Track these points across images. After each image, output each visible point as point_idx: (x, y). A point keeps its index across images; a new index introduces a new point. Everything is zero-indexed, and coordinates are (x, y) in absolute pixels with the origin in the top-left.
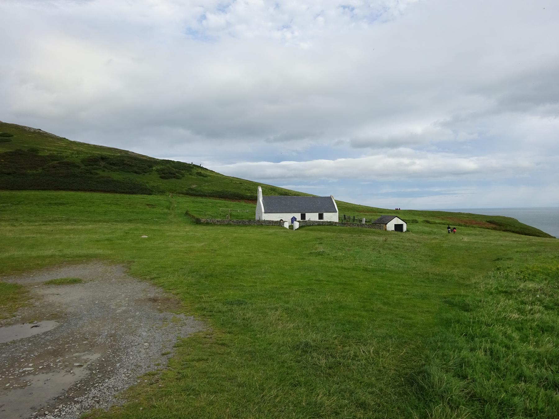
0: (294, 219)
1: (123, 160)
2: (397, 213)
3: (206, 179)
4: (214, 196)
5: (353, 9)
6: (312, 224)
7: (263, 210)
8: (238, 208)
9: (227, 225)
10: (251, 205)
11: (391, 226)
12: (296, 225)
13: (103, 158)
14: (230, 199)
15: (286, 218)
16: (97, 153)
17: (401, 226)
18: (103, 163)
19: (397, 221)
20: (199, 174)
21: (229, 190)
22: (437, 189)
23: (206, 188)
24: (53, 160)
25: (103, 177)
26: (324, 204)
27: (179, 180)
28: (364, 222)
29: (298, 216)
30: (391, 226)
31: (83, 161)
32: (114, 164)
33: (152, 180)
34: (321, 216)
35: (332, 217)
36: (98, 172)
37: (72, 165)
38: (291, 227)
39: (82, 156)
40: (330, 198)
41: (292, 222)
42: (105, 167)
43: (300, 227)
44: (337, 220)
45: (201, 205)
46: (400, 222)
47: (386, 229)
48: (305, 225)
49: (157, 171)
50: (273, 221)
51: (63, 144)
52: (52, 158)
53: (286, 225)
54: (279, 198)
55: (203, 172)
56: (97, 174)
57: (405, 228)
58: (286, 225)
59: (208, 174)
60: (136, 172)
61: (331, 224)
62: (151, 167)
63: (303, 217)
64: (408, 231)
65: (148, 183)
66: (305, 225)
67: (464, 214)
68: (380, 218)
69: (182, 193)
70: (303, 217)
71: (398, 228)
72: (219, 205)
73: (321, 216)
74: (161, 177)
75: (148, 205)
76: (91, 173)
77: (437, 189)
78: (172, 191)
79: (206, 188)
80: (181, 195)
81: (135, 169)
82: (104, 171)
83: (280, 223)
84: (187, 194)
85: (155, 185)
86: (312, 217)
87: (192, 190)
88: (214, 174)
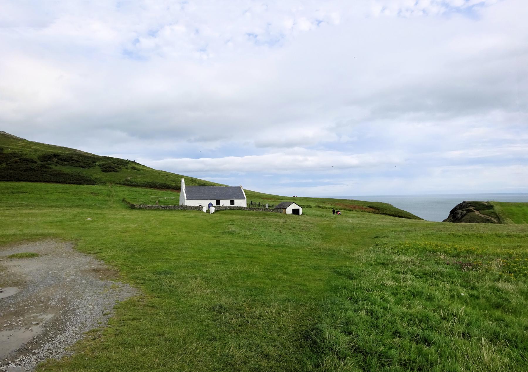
0: (210, 205)
1: (72, 157)
2: (294, 199)
3: (139, 172)
4: (145, 186)
5: (256, 36)
6: (225, 209)
7: (186, 198)
8: (165, 196)
9: (156, 210)
10: (175, 193)
11: (289, 210)
12: (213, 210)
13: (56, 156)
14: (158, 188)
15: (204, 203)
16: (51, 151)
17: (298, 209)
18: (55, 160)
19: (294, 206)
20: (134, 168)
21: (158, 181)
22: (327, 180)
23: (139, 179)
24: (15, 157)
25: (55, 171)
26: (234, 193)
27: (117, 173)
28: (267, 207)
29: (214, 202)
30: (289, 210)
31: (39, 158)
32: (65, 160)
33: (95, 173)
34: (232, 203)
36: (51, 166)
37: (27, 161)
38: (208, 211)
39: (38, 154)
40: (239, 188)
41: (209, 207)
42: (57, 162)
43: (216, 211)
45: (135, 193)
46: (296, 207)
47: (285, 213)
48: (220, 210)
49: (100, 165)
50: (193, 207)
51: (23, 144)
52: (14, 155)
53: (205, 210)
54: (199, 187)
55: (136, 166)
56: (50, 168)
57: (301, 212)
58: (205, 210)
59: (141, 168)
60: (82, 167)
61: (240, 208)
62: (94, 162)
63: (218, 203)
64: (303, 214)
65: (92, 175)
66: (220, 210)
67: (349, 200)
68: (279, 204)
69: (120, 184)
70: (218, 203)
71: (296, 212)
72: (149, 193)
73: (232, 203)
74: (103, 171)
75: (92, 193)
76: (46, 168)
77: (327, 180)
78: (112, 182)
79: (139, 179)
80: (119, 185)
81: (82, 164)
82: (56, 166)
83: (199, 208)
84: (124, 184)
85: (98, 177)
86: (225, 203)
87: (128, 181)
88: (146, 168)
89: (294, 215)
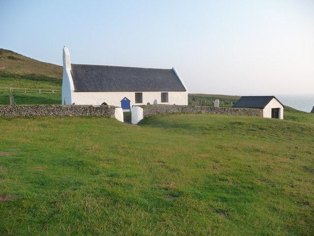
11: (267, 113)
15: (113, 98)
34: (164, 98)
35: (178, 99)
38: (128, 117)
44: (215, 106)
50: (91, 107)
53: (119, 115)
58: (119, 115)
61: (183, 109)
73: (164, 98)
83: (105, 110)
89: (127, 124)
